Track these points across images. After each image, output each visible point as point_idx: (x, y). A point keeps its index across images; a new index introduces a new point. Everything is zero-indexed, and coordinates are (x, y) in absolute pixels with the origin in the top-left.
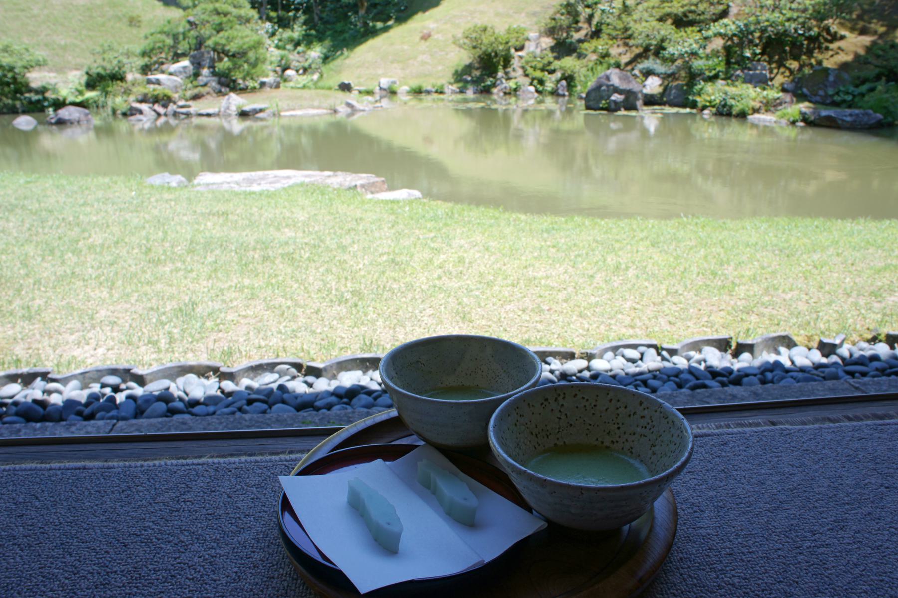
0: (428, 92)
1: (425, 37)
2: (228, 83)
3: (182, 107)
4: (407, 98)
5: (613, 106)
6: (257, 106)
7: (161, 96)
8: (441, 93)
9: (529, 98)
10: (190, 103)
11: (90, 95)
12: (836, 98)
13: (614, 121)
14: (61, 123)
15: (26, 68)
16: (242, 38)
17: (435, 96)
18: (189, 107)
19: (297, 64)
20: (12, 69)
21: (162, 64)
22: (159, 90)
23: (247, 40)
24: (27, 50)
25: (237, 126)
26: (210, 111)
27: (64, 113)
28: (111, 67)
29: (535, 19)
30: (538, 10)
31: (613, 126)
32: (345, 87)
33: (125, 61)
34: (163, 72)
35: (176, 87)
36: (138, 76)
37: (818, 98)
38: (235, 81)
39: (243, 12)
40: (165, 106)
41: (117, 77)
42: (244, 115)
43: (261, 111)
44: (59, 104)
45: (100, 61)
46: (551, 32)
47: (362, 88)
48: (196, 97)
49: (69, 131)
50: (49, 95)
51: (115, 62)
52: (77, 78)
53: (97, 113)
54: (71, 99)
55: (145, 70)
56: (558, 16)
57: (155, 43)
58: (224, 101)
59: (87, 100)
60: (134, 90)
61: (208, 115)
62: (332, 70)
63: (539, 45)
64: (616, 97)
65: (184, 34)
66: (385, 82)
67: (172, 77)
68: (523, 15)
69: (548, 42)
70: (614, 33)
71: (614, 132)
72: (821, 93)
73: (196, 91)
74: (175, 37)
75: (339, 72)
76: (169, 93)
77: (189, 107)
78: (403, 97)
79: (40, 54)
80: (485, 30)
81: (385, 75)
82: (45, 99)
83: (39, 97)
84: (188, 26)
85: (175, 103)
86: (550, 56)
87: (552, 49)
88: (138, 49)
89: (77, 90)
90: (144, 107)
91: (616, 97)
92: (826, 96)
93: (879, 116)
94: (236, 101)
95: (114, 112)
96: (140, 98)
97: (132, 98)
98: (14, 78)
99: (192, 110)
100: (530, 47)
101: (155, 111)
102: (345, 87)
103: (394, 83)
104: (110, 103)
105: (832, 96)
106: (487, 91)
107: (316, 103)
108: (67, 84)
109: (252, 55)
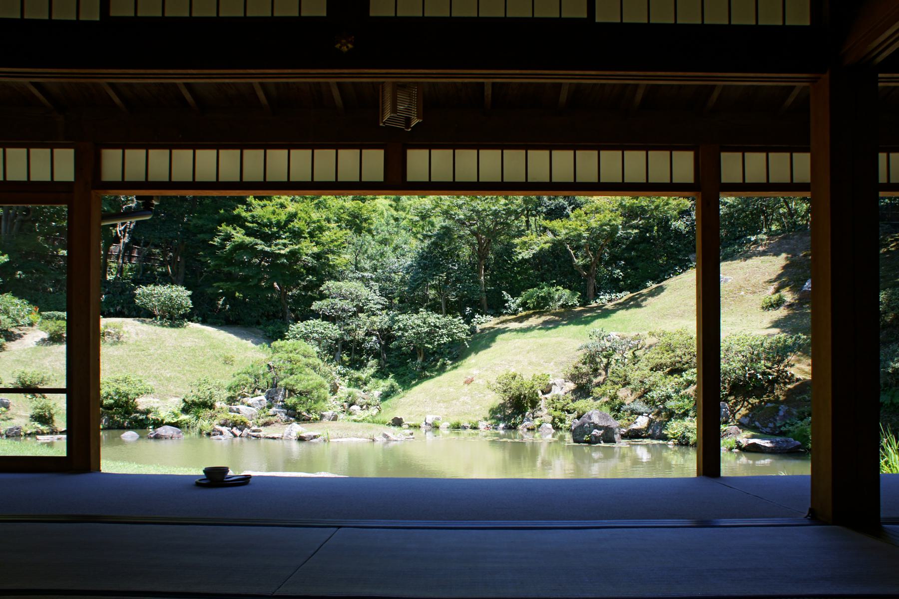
0: (465, 428)
1: (469, 382)
2: (293, 414)
3: (254, 431)
4: (447, 432)
5: (593, 439)
6: (313, 434)
7: (239, 422)
8: (475, 428)
9: (547, 435)
10: (261, 428)
11: (184, 417)
12: (783, 429)
13: (595, 451)
14: (157, 437)
15: (138, 395)
16: (308, 380)
17: (469, 431)
18: (260, 431)
19: (362, 400)
20: (126, 395)
21: (244, 396)
22: (238, 417)
23: (311, 382)
24: (140, 381)
25: (295, 446)
26: (276, 436)
27: (161, 431)
28: (203, 396)
29: (562, 367)
30: (565, 359)
31: (596, 455)
32: (398, 422)
33: (215, 392)
34: (243, 403)
35: (252, 415)
36: (224, 405)
37: (768, 430)
38: (299, 413)
39: (311, 361)
40: (241, 430)
41: (206, 405)
42: (301, 439)
43: (315, 437)
44: (158, 424)
45: (195, 391)
46: (573, 378)
47: (412, 423)
48: (266, 424)
49: (162, 443)
50: (151, 416)
51: (208, 393)
52: (176, 404)
53: (187, 433)
54: (168, 420)
55: (231, 400)
56: (580, 365)
57: (240, 381)
58: (288, 428)
59: (181, 421)
60: (219, 415)
61: (274, 438)
62: (388, 406)
63: (563, 388)
64: (595, 432)
65: (263, 375)
66: (430, 419)
67: (251, 408)
68: (552, 364)
69: (571, 386)
70: (617, 380)
71: (596, 461)
72: (771, 425)
73: (267, 419)
74: (257, 377)
75: (394, 409)
76: (246, 420)
77: (260, 431)
78: (444, 431)
79: (150, 384)
80: (514, 377)
81: (431, 413)
82: (147, 418)
83: (144, 417)
84: (267, 369)
85: (249, 428)
86: (570, 397)
87: (574, 392)
88: (227, 383)
89: (174, 414)
90: (225, 429)
91: (595, 432)
92: (775, 427)
93: (798, 443)
94: (297, 429)
95: (201, 432)
96: (222, 422)
97: (216, 422)
98: (127, 402)
99: (261, 434)
100: (556, 391)
101: (232, 433)
102: (398, 422)
103: (438, 419)
104: (199, 425)
105: (780, 427)
106: (514, 427)
107: (359, 434)
108: (165, 407)
109: (315, 394)
